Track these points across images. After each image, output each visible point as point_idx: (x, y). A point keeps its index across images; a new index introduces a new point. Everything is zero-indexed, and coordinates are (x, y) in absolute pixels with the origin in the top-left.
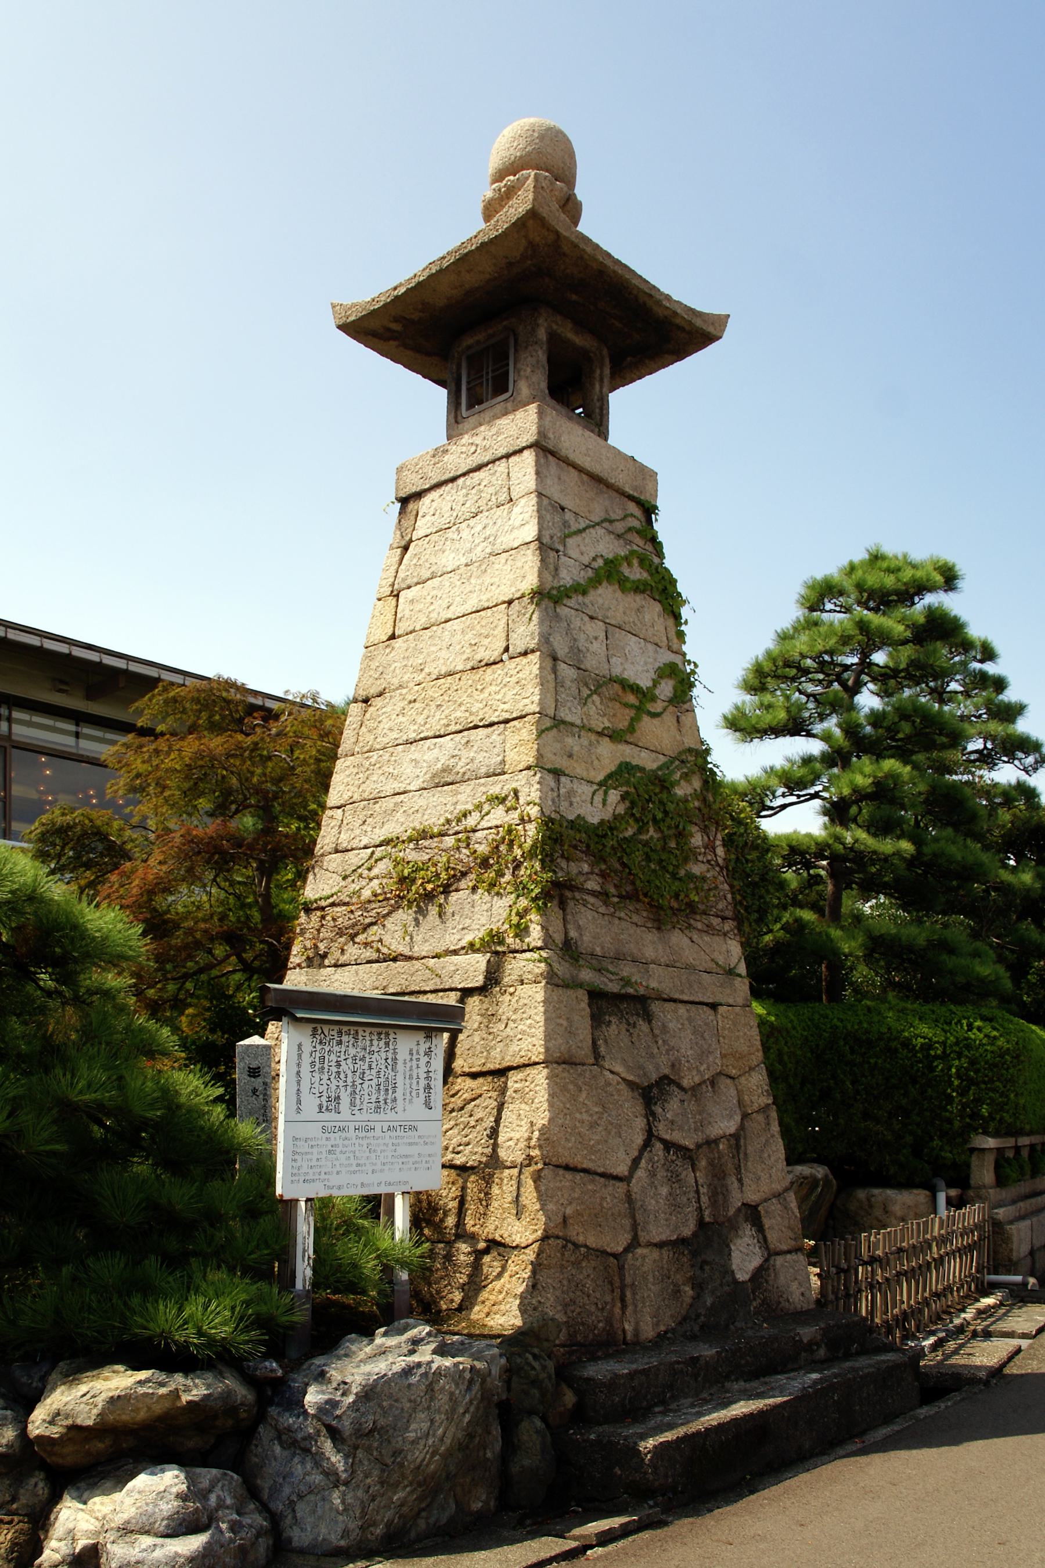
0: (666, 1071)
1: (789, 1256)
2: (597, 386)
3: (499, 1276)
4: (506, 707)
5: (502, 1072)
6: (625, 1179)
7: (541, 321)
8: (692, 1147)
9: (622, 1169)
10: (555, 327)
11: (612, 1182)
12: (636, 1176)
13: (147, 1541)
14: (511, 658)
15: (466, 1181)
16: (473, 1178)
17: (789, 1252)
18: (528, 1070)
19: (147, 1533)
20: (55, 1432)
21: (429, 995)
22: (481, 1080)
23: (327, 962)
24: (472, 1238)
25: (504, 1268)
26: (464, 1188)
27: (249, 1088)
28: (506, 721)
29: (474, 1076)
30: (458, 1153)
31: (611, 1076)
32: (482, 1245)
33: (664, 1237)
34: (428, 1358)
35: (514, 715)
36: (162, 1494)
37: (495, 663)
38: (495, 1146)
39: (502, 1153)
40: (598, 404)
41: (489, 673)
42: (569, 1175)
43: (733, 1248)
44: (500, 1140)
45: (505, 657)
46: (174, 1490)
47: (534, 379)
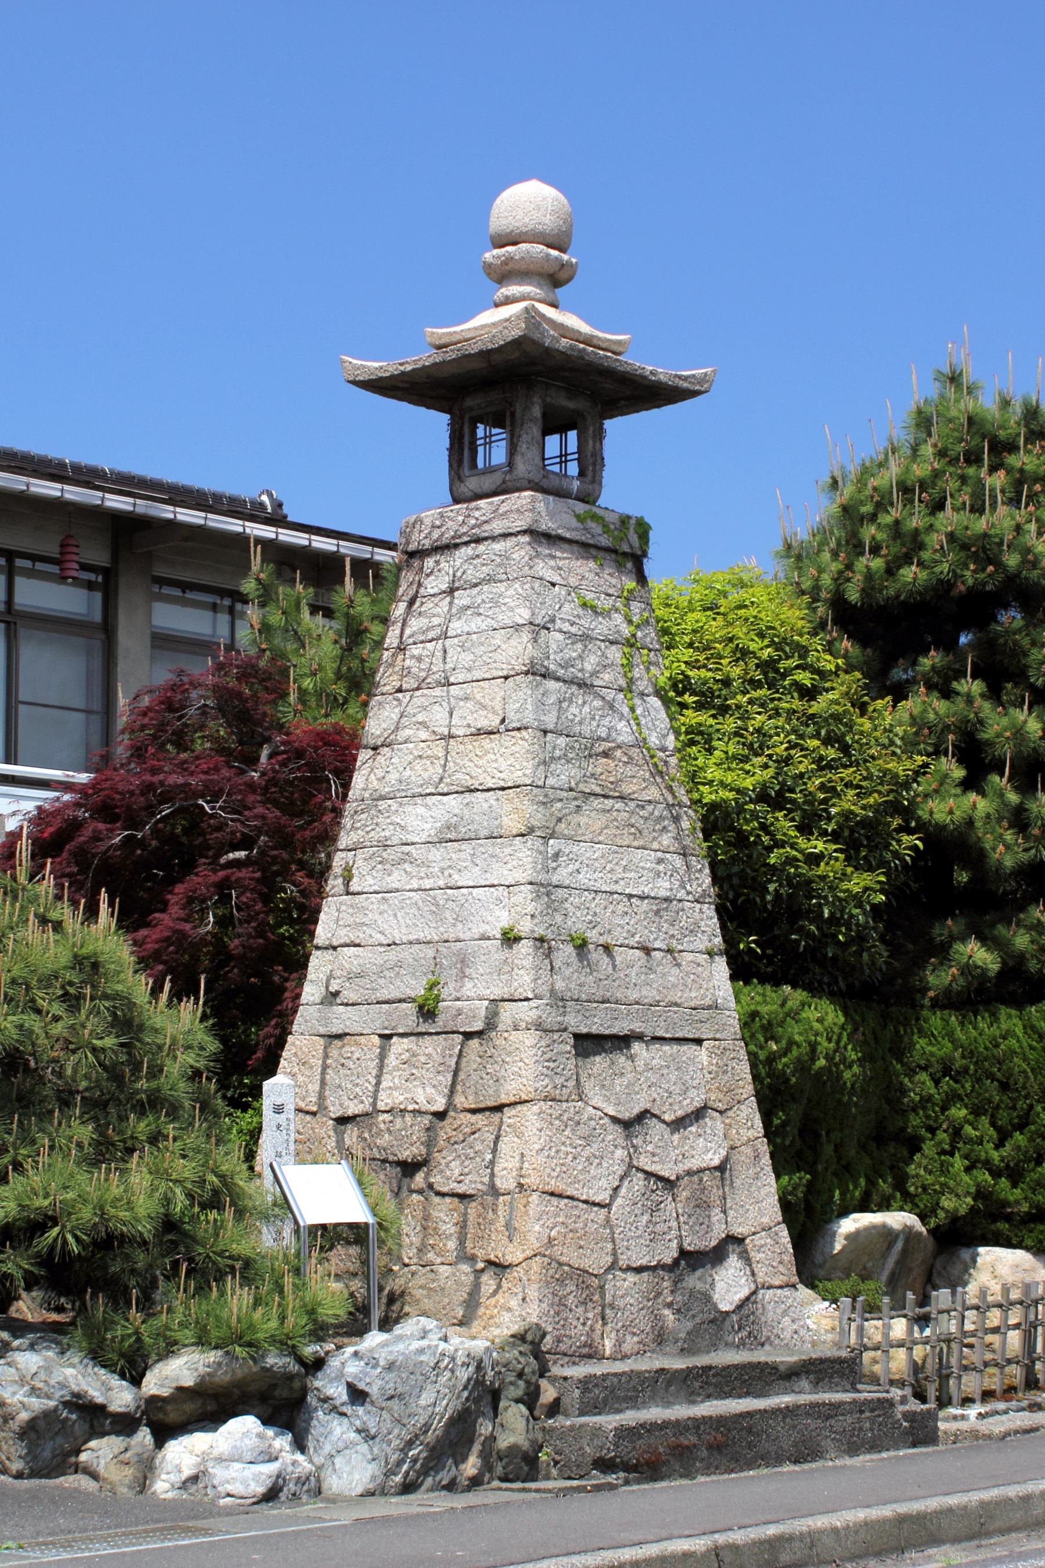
0: (648, 1106)
1: (779, 1291)
2: (591, 442)
3: (495, 1293)
4: (501, 775)
5: (499, 1108)
6: (607, 1206)
7: (535, 399)
8: (673, 1178)
9: (603, 1197)
10: (548, 399)
11: (596, 1209)
12: (616, 1204)
13: (237, 1466)
14: (508, 730)
15: (466, 1209)
16: (473, 1204)
17: (781, 1287)
18: (519, 1107)
19: (237, 1461)
20: (165, 1392)
21: (398, 632)
22: (480, 1116)
23: (339, 1001)
24: (473, 1259)
25: (499, 1286)
26: (465, 1214)
27: (274, 1124)
28: (503, 789)
29: (474, 1111)
30: (459, 1182)
31: (594, 1111)
32: (481, 1265)
33: (644, 1262)
34: (436, 1343)
35: (510, 784)
36: (245, 1435)
37: (491, 733)
38: (492, 1175)
39: (498, 1182)
40: (591, 461)
41: (486, 742)
42: (555, 1201)
43: (717, 1278)
44: (496, 1169)
45: (502, 728)
46: (254, 1431)
47: (529, 455)
